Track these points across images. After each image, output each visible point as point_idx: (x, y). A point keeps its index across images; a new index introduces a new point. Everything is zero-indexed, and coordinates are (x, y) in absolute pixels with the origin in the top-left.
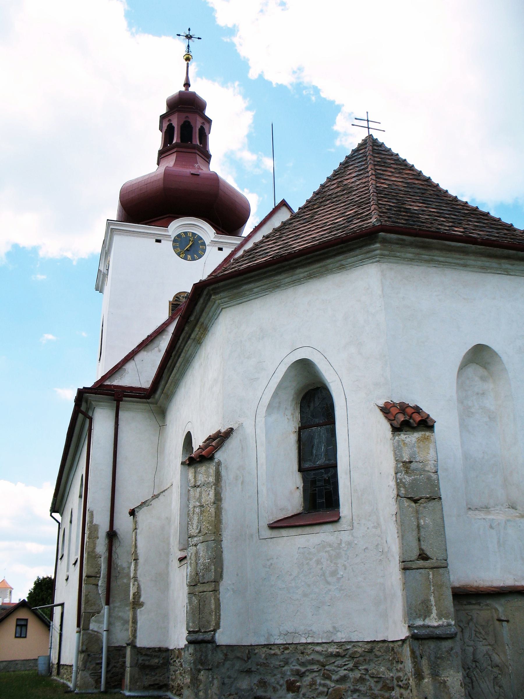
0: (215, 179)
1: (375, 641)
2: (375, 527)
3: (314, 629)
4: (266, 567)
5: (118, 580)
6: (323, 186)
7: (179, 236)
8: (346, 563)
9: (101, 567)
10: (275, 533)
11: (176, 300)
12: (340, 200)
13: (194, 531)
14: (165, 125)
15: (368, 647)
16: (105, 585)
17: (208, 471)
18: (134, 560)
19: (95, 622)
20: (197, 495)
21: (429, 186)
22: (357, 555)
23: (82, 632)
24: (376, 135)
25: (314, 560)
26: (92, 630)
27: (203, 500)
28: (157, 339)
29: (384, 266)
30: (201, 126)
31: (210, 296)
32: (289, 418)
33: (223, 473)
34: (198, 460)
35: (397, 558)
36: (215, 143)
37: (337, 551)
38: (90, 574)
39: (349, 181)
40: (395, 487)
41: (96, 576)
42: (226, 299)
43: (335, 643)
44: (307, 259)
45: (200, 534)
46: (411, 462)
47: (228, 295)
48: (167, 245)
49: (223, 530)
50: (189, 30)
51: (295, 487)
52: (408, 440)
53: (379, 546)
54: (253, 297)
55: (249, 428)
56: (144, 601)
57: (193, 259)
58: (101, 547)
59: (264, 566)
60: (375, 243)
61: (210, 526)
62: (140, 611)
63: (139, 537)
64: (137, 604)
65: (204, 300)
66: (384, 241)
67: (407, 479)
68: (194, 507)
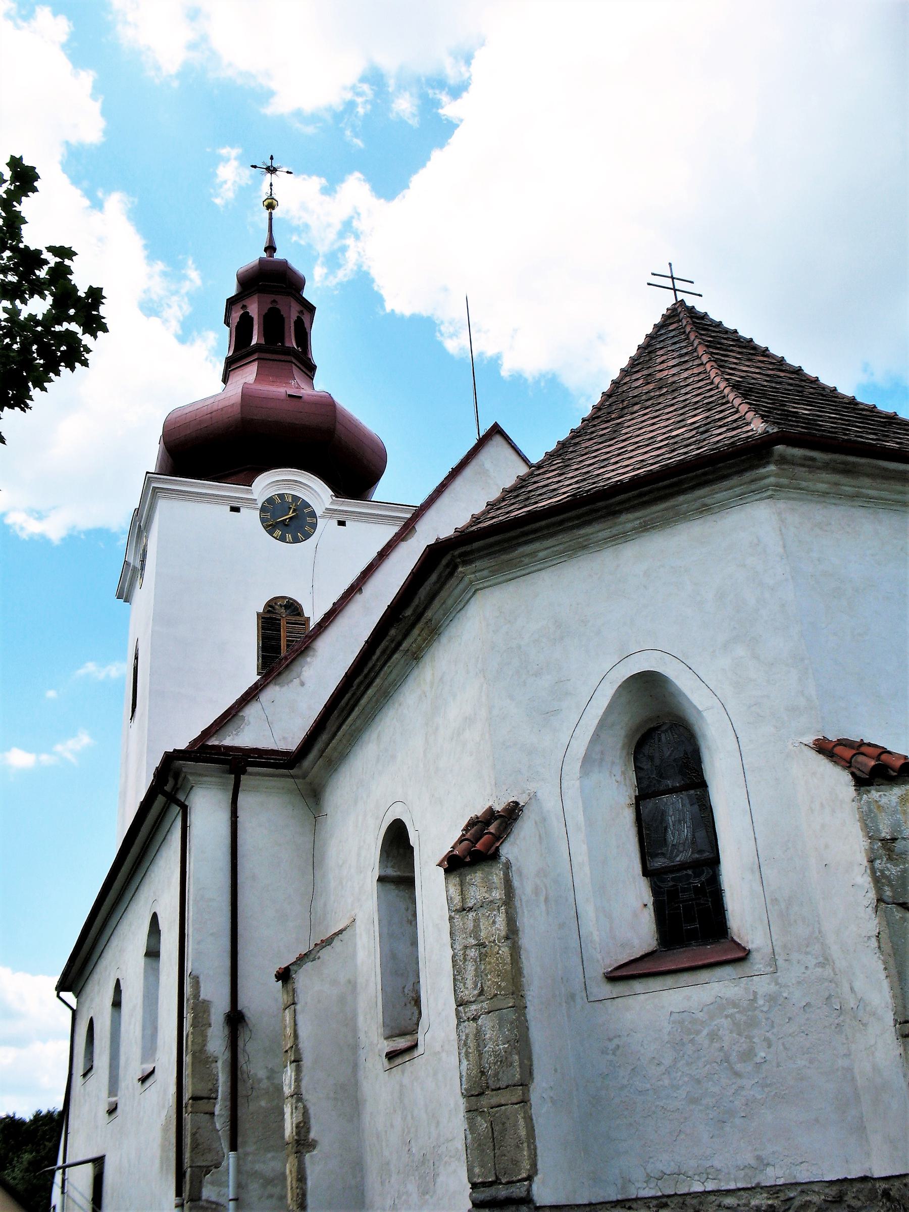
0: (328, 406)
1: (846, 1180)
2: (821, 965)
3: (717, 1164)
4: (608, 1054)
5: (251, 1104)
6: (616, 383)
7: (270, 500)
8: (768, 1034)
9: (217, 1080)
10: (620, 988)
11: (269, 612)
12: (660, 403)
13: (469, 993)
14: (236, 316)
15: (833, 1191)
16: (227, 1113)
17: (489, 880)
18: (294, 1061)
19: (212, 1183)
20: (470, 925)
21: (804, 381)
22: (790, 1019)
23: (187, 1206)
24: (690, 301)
25: (705, 1032)
26: (208, 1201)
27: (483, 934)
28: (297, 663)
29: (781, 505)
31: (456, 567)
32: (619, 779)
33: (516, 883)
34: (468, 859)
35: (889, 1018)
36: (320, 346)
37: (750, 1013)
38: (199, 1094)
39: (666, 373)
40: (872, 885)
41: (211, 1098)
42: (485, 573)
43: (762, 1188)
44: (641, 495)
45: (482, 998)
46: (894, 840)
47: (489, 565)
48: (251, 518)
49: (526, 988)
50: (272, 158)
51: (640, 905)
52: (884, 801)
53: (833, 1000)
54: (535, 568)
55: (549, 800)
56: (316, 1139)
57: (296, 540)
58: (217, 1042)
59: (604, 1052)
60: (768, 463)
61: (502, 981)
62: (311, 1156)
63: (300, 1019)
64: (303, 1143)
65: (440, 577)
66: (783, 461)
67: (893, 870)
68: (466, 947)
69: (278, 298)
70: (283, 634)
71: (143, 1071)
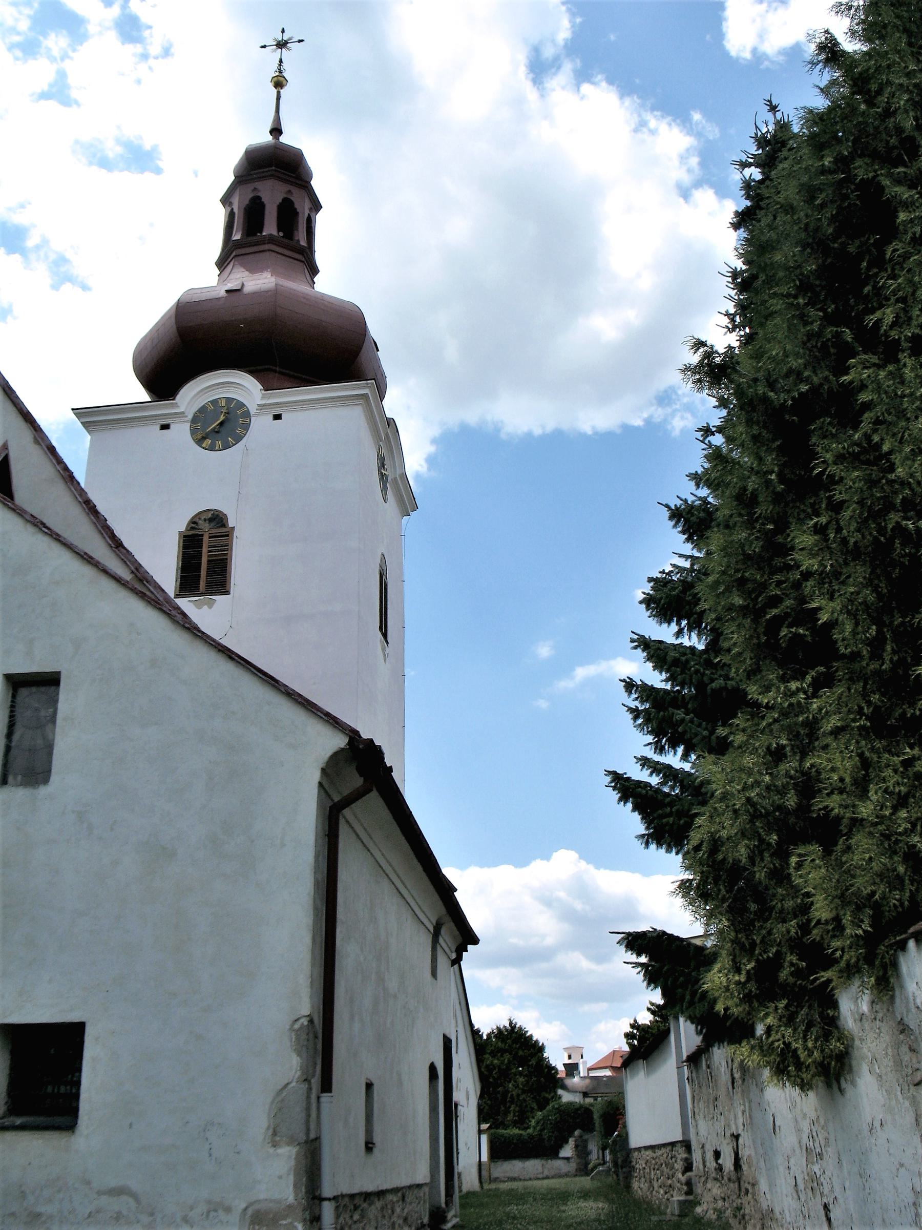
7: (202, 410)
48: (181, 432)
50: (283, 31)
57: (226, 446)
69: (257, 185)
70: (205, 550)
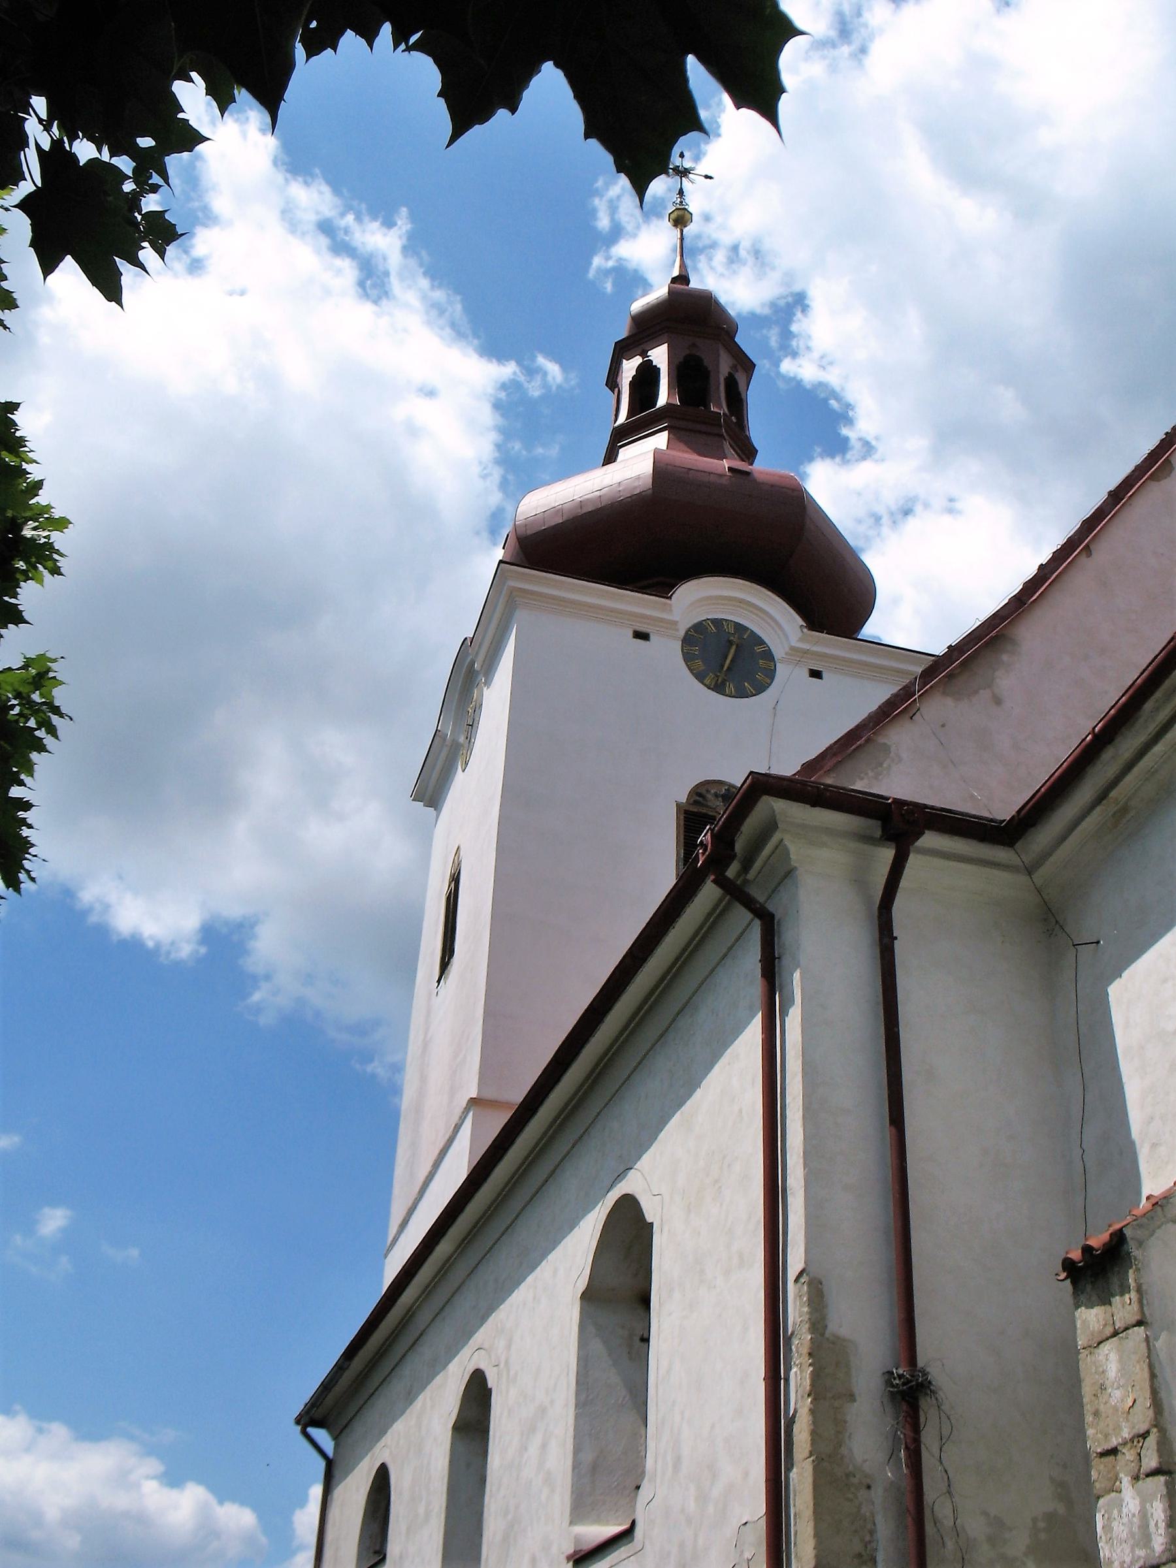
7: (699, 628)
9: (872, 1532)
11: (696, 803)
30: (730, 374)
48: (667, 650)
57: (742, 694)
58: (868, 1437)
71: (577, 1539)
